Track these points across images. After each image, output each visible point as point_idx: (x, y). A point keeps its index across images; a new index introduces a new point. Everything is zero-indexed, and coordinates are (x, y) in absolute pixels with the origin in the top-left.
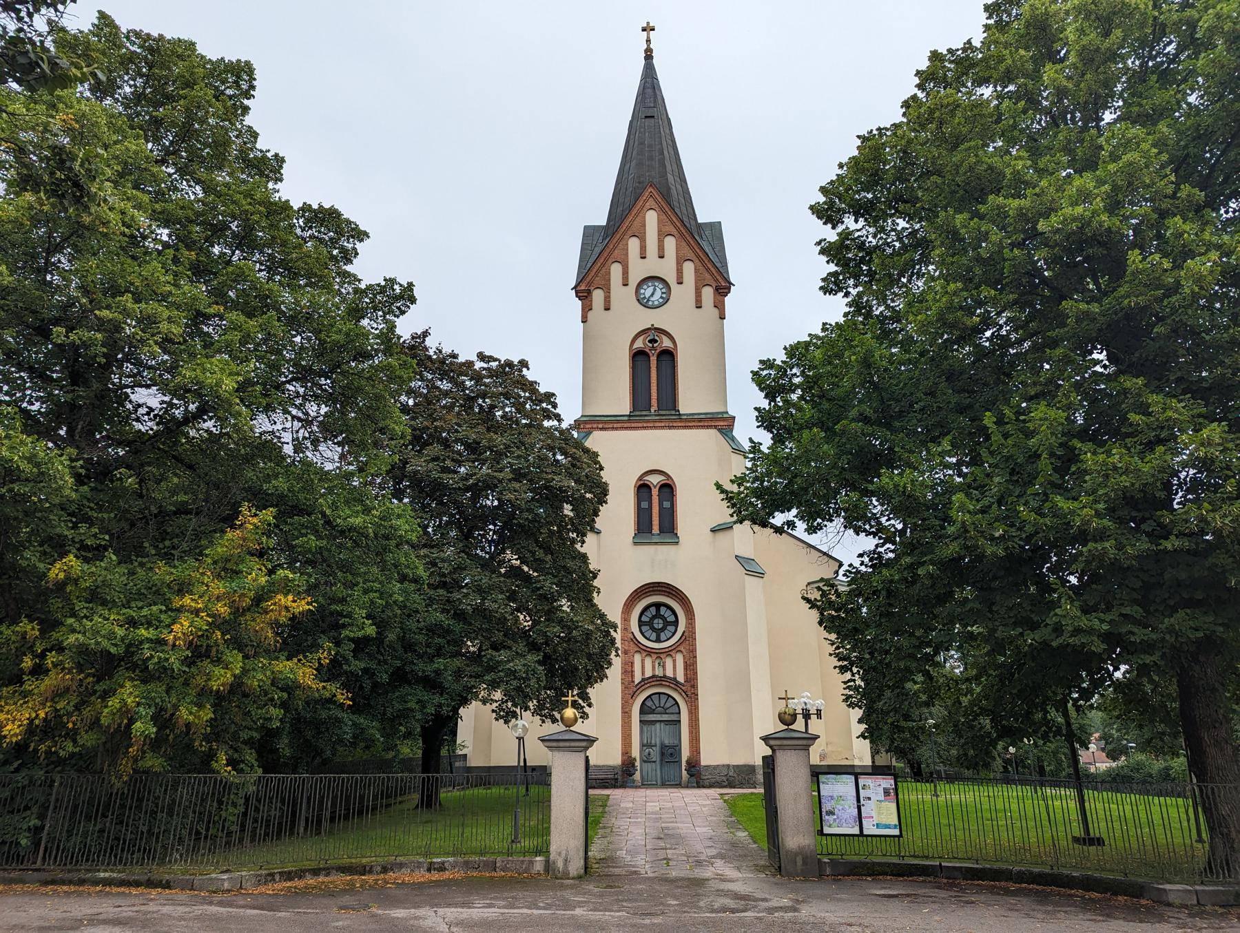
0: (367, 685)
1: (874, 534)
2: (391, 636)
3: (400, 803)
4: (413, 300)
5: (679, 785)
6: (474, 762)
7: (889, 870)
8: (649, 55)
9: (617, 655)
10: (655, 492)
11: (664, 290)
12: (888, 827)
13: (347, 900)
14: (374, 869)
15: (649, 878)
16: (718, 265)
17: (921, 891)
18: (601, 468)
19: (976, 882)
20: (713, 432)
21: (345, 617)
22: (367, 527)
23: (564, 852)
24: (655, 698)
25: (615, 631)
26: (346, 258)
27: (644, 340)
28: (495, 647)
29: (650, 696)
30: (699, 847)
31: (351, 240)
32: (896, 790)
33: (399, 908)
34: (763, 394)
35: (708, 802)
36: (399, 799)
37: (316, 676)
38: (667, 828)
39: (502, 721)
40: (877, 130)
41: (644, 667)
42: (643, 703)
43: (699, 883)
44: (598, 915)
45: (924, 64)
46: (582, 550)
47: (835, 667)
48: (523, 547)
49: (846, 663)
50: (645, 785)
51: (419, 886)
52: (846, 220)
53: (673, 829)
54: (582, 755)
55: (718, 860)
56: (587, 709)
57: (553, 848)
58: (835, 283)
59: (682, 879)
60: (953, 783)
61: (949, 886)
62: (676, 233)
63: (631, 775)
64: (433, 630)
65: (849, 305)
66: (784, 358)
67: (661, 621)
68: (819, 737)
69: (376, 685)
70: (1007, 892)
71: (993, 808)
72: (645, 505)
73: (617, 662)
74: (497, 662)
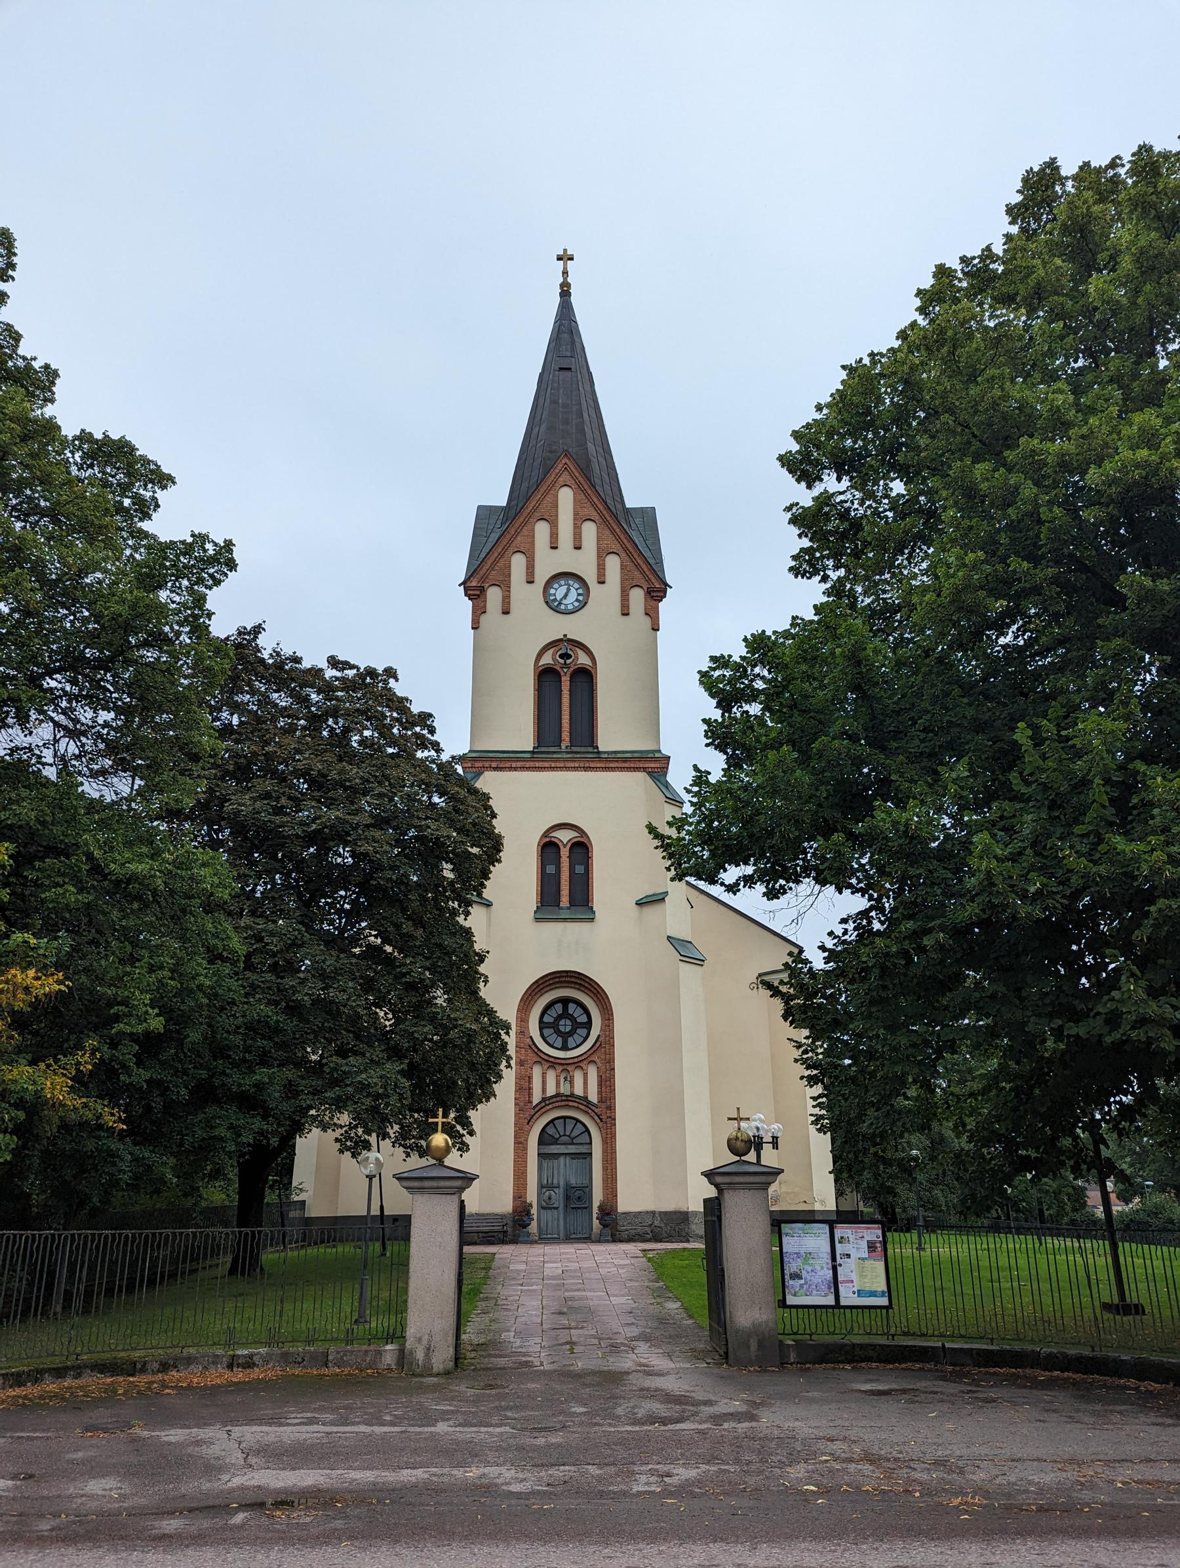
0: (157, 1103)
1: (863, 892)
2: (194, 1036)
3: (210, 1266)
4: (232, 565)
5: (588, 1239)
6: (313, 1211)
7: (871, 1353)
8: (565, 291)
9: (509, 1066)
10: (565, 853)
11: (580, 591)
12: (873, 1294)
13: (102, 1415)
14: (148, 1366)
15: (544, 1372)
16: (652, 561)
17: (921, 1385)
18: (494, 816)
19: (992, 1370)
20: (641, 776)
21: (119, 1004)
22: (155, 876)
23: (426, 1337)
24: (559, 1123)
25: (507, 1033)
26: (142, 512)
27: (554, 655)
28: (343, 1053)
29: (552, 1121)
30: (615, 1325)
31: (150, 486)
32: (884, 1243)
33: (172, 1426)
34: (714, 702)
35: (628, 1262)
36: (208, 1263)
37: (71, 1087)
38: (572, 1299)
39: (348, 1154)
40: (869, 355)
41: (544, 1083)
42: (543, 1130)
43: (615, 1378)
44: (469, 1433)
45: (927, 282)
46: (467, 924)
47: (802, 1078)
48: (384, 918)
49: (815, 1072)
50: (544, 1238)
51: (213, 1391)
52: (825, 477)
53: (581, 1299)
54: (455, 1198)
55: (641, 1344)
56: (467, 1139)
57: (411, 1332)
58: (809, 562)
59: (593, 1373)
60: (934, 1231)
61: (957, 1377)
62: (597, 518)
63: (526, 1226)
64: (254, 1028)
65: (827, 593)
66: (744, 652)
67: (568, 1022)
68: (782, 1171)
69: (168, 1106)
70: (1036, 1384)
71: (994, 1265)
72: (550, 869)
73: (509, 1077)
74: (344, 1073)
